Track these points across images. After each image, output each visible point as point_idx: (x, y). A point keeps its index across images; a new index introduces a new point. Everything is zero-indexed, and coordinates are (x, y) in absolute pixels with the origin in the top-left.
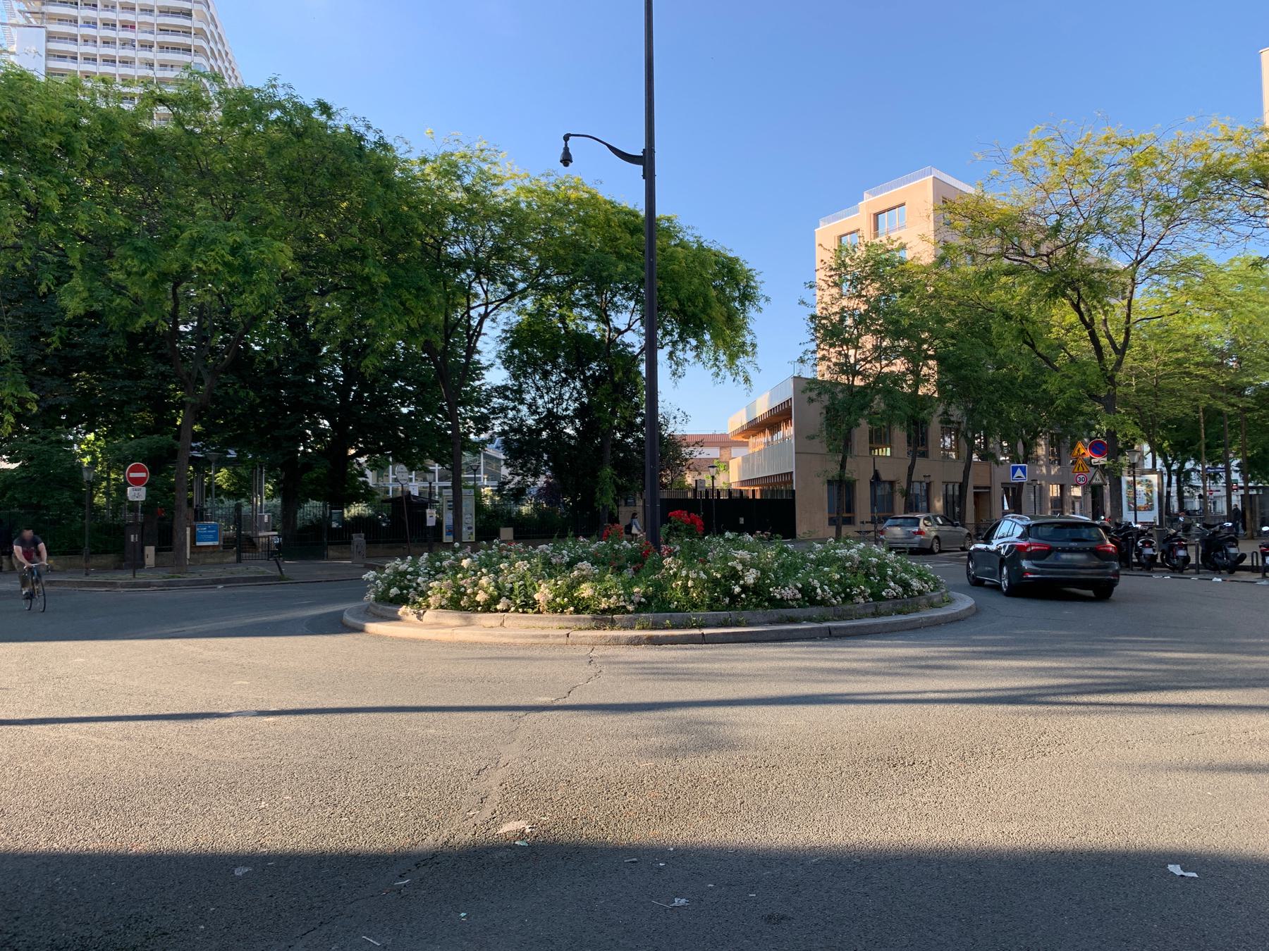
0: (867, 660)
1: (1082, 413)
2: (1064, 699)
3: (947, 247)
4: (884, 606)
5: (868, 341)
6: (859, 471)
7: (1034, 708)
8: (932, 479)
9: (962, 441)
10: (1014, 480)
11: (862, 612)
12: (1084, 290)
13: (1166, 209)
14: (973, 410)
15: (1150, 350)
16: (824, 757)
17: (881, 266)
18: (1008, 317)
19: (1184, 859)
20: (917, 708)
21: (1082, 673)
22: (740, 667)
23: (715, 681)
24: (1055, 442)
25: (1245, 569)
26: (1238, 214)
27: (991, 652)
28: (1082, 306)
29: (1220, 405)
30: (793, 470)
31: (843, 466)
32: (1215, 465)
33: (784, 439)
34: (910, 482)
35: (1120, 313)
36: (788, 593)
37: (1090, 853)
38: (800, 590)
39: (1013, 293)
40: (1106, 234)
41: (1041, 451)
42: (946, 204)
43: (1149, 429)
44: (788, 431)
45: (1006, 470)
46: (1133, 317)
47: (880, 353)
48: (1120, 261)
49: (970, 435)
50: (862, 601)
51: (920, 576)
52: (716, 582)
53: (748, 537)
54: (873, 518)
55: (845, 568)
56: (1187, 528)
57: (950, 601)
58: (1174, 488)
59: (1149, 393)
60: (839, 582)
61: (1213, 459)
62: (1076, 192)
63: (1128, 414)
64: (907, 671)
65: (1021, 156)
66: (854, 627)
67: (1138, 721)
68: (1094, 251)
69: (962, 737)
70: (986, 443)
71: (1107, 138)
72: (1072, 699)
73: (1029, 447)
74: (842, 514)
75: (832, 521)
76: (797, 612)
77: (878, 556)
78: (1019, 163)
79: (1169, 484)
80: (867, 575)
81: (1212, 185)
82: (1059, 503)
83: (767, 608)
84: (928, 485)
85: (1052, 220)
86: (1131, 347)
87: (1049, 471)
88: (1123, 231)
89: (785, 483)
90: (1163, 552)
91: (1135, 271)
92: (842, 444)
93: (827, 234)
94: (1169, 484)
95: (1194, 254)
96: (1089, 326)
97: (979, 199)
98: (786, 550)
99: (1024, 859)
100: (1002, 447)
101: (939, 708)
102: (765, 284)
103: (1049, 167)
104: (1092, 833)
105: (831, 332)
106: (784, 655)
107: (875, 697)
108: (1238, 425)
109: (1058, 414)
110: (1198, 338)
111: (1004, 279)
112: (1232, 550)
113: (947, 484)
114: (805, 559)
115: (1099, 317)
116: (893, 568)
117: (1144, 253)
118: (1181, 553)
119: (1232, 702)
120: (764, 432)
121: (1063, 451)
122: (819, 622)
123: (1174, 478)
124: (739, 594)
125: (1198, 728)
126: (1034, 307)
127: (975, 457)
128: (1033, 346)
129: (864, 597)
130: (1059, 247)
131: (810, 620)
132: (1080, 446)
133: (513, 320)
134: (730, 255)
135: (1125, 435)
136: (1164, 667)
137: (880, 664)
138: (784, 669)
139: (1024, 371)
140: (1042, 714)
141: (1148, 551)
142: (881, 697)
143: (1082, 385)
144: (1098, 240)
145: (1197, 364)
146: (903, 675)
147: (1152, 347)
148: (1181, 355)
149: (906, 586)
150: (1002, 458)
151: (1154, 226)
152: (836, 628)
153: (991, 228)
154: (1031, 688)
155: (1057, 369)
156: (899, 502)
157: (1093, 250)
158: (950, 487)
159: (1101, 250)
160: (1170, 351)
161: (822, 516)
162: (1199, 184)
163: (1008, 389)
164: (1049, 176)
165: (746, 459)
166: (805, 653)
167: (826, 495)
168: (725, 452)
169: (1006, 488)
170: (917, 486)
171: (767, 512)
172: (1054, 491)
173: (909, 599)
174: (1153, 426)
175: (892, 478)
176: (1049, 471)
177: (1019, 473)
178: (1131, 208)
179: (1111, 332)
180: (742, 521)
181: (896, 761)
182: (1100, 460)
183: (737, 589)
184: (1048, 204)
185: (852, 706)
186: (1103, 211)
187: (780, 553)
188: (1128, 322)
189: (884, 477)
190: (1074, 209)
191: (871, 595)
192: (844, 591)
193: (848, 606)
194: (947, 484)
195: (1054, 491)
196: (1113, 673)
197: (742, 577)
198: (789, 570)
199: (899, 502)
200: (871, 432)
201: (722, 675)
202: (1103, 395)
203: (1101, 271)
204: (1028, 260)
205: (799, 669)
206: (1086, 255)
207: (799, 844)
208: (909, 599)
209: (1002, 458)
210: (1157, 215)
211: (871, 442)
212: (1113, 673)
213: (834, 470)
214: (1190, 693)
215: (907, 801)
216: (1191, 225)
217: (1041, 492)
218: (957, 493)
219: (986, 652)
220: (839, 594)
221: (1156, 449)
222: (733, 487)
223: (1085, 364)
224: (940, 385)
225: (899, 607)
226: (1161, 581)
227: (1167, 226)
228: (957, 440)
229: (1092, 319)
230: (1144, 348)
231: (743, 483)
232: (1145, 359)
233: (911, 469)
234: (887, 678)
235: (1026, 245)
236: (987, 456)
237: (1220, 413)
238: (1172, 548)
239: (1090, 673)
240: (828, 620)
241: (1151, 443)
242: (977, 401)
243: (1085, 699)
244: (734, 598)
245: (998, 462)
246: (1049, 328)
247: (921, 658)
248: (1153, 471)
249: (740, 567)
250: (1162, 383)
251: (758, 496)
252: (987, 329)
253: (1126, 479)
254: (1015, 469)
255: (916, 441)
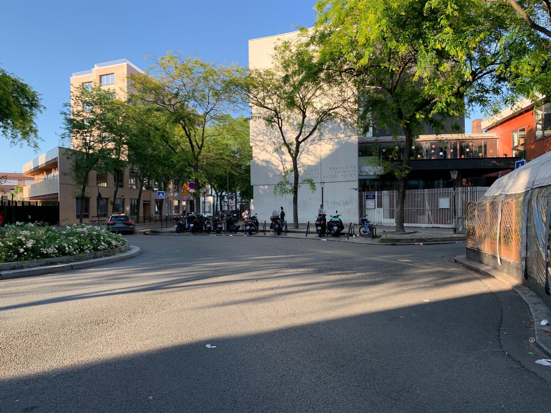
0: (90, 278)
1: (186, 172)
2: (177, 285)
3: (132, 96)
4: (99, 253)
5: (96, 133)
6: (92, 193)
7: (161, 291)
8: (125, 197)
9: (138, 180)
10: (159, 198)
11: (88, 257)
12: (187, 122)
13: (216, 94)
14: (143, 168)
15: (211, 149)
16: (63, 326)
17: (103, 99)
18: (157, 129)
19: (212, 341)
20: (111, 297)
21: (181, 274)
22: (21, 288)
23: (6, 297)
24: (176, 183)
25: (240, 231)
26: (240, 100)
27: (167, 274)
28: (186, 128)
29: (233, 172)
30: (59, 192)
31: (84, 190)
32: (232, 194)
33: (54, 176)
34: (115, 198)
35: (200, 133)
36: (50, 250)
37: (178, 346)
38: (57, 249)
39: (160, 119)
40: (195, 100)
41: (171, 186)
42: (132, 76)
43: (211, 178)
44: (56, 173)
45: (157, 194)
46: (205, 135)
47: (102, 140)
48: (200, 112)
49: (141, 178)
50: (89, 252)
51: (116, 239)
52: (10, 247)
53: (31, 225)
54: (98, 214)
55: (80, 237)
56: (222, 217)
57: (130, 249)
58: (219, 202)
59: (210, 165)
60: (77, 243)
61: (231, 191)
62: (185, 81)
63: (203, 173)
64: (108, 281)
65: (164, 62)
66: (84, 264)
67: (200, 291)
68: (190, 105)
69: (130, 307)
70: (148, 182)
71: (196, 61)
72: (177, 285)
73: (166, 185)
74: (83, 212)
75: (78, 217)
76: (55, 259)
77: (97, 231)
78: (162, 65)
79: (217, 201)
80: (91, 240)
81: (232, 87)
82: (177, 208)
83: (39, 258)
84: (124, 200)
85: (175, 91)
86: (204, 147)
87: (174, 195)
88: (201, 100)
89: (54, 198)
90: (214, 226)
91: (205, 116)
92: (85, 181)
93: (77, 80)
94: (217, 201)
95: (226, 114)
96: (189, 136)
97: (145, 77)
98: (51, 230)
99: (152, 354)
100: (155, 184)
101: (121, 296)
102: (43, 100)
103: (174, 68)
104: (179, 338)
105: (76, 126)
106: (47, 280)
107: (92, 295)
108: (240, 179)
109: (178, 171)
110: (227, 145)
111: (155, 112)
112: (236, 224)
113: (131, 199)
114: (61, 234)
115: (193, 133)
116: (104, 236)
117: (209, 110)
118: (220, 226)
119: (232, 279)
120: (43, 173)
121: (179, 187)
122: (67, 263)
123: (219, 198)
124: (23, 253)
125: (220, 290)
126: (168, 126)
127: (144, 188)
128: (167, 142)
129: (90, 250)
130: (177, 102)
131: (62, 262)
132: (185, 185)
133: (71, 163)
134: (24, 82)
135: (202, 181)
136: (211, 269)
137: (95, 280)
138: (46, 287)
139: (163, 153)
140: (164, 293)
141: (208, 226)
142: (94, 294)
143: (186, 160)
144: (192, 102)
145: (227, 155)
146: (106, 283)
147: (211, 147)
148: (221, 151)
149: (109, 244)
150: (155, 189)
151: (212, 100)
152: (75, 265)
153: (151, 90)
154: (161, 283)
155: (176, 153)
156: (110, 207)
157: (191, 105)
158: (133, 201)
159: (193, 106)
160: (218, 149)
161: (74, 214)
162: (227, 86)
163: (158, 160)
164: (175, 72)
165: (33, 186)
166: (59, 278)
167: (75, 204)
168: (21, 182)
169: (156, 201)
170: (118, 200)
171: (44, 212)
172: (176, 203)
173: (111, 249)
174: (211, 179)
175: (107, 197)
176: (174, 195)
177: (161, 195)
178: (204, 91)
179: (197, 140)
180: (30, 217)
181: (99, 322)
182: (192, 191)
183: (22, 250)
184: (174, 84)
185: (80, 300)
186: (194, 90)
187: (47, 231)
188: (203, 136)
189: (103, 196)
190: (184, 88)
191: (93, 249)
192: (80, 248)
193: (82, 255)
194: (131, 199)
195: (176, 203)
196: (192, 273)
197: (25, 244)
198: (52, 239)
199: (110, 207)
200: (97, 176)
201: (10, 293)
202: (194, 164)
203: (193, 115)
204: (166, 106)
205: (54, 286)
206: (188, 107)
207: (46, 369)
208: (111, 249)
209: (155, 189)
210: (213, 96)
211: (97, 180)
212: (192, 273)
213: (79, 192)
214: (219, 278)
215: (103, 339)
216: (225, 102)
217: (171, 203)
218: (136, 204)
219: (143, 270)
220: (77, 249)
221: (212, 186)
222: (25, 200)
223: (187, 152)
224: (129, 156)
225: (106, 253)
226: (213, 236)
227: (217, 100)
228: (136, 180)
229: (190, 134)
230: (209, 147)
231: (31, 198)
232: (209, 152)
233: (116, 192)
234: (98, 285)
235: (166, 100)
236: (149, 188)
237: (234, 175)
238: (217, 224)
239: (183, 274)
240: (71, 262)
241: (211, 185)
242: (144, 164)
243: (181, 285)
244: (20, 255)
245: (153, 191)
246: (174, 135)
247: (115, 275)
248: (211, 195)
249: (24, 239)
250: (215, 161)
251: (39, 204)
252: (149, 135)
253: (202, 199)
254: (159, 193)
255: (118, 180)
